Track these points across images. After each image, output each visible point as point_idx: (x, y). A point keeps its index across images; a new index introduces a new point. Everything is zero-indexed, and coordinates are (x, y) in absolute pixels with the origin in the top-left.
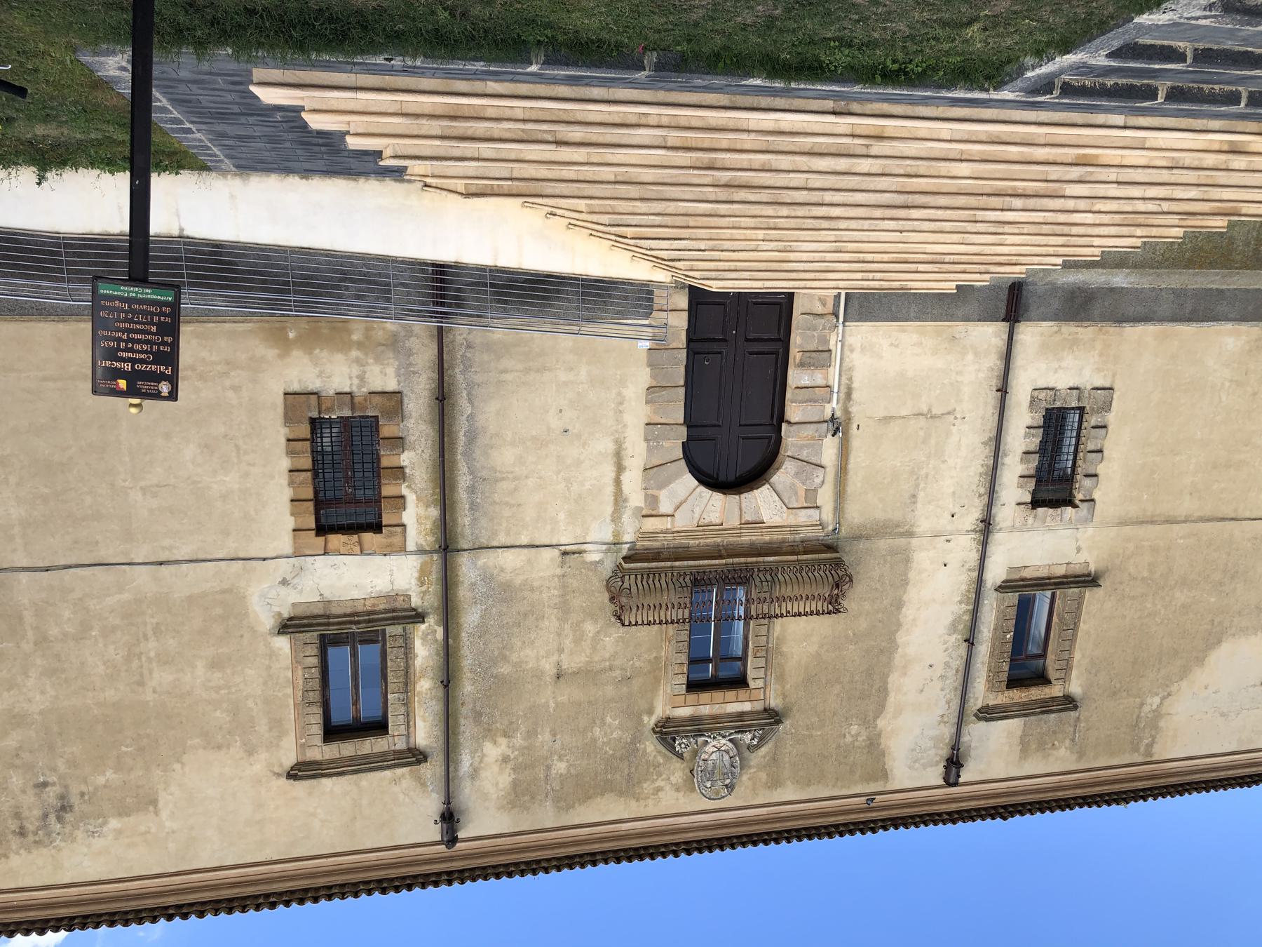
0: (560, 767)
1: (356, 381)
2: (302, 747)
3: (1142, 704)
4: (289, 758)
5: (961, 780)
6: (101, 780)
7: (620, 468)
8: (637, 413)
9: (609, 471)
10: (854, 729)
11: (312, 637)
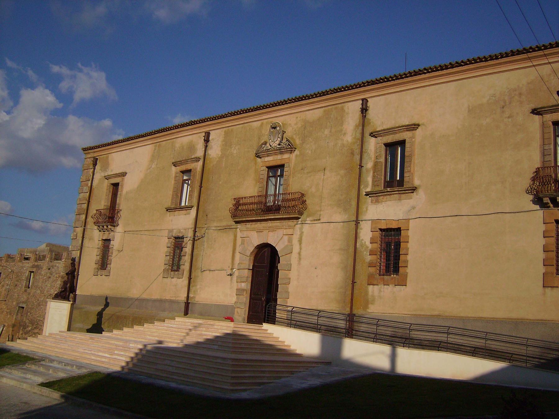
0: (327, 132)
1: (382, 290)
2: (413, 137)
3: (157, 165)
4: (419, 131)
5: (204, 134)
6: (488, 120)
7: (299, 254)
8: (293, 274)
9: (303, 253)
10: (235, 152)
11: (406, 185)
